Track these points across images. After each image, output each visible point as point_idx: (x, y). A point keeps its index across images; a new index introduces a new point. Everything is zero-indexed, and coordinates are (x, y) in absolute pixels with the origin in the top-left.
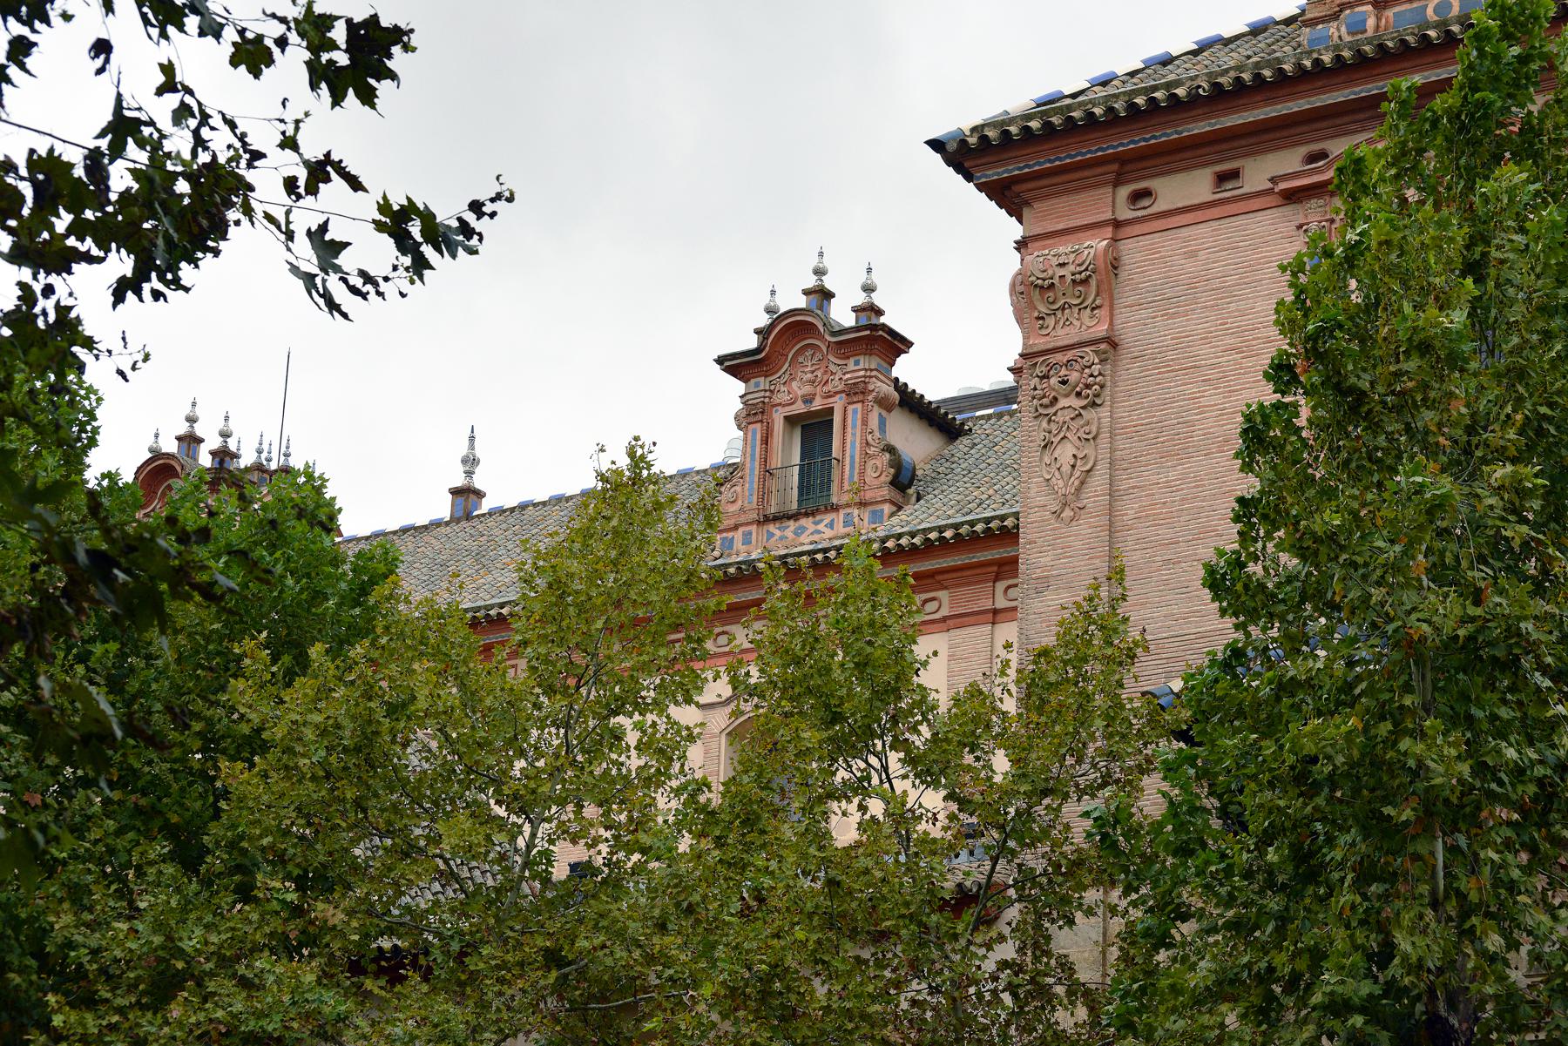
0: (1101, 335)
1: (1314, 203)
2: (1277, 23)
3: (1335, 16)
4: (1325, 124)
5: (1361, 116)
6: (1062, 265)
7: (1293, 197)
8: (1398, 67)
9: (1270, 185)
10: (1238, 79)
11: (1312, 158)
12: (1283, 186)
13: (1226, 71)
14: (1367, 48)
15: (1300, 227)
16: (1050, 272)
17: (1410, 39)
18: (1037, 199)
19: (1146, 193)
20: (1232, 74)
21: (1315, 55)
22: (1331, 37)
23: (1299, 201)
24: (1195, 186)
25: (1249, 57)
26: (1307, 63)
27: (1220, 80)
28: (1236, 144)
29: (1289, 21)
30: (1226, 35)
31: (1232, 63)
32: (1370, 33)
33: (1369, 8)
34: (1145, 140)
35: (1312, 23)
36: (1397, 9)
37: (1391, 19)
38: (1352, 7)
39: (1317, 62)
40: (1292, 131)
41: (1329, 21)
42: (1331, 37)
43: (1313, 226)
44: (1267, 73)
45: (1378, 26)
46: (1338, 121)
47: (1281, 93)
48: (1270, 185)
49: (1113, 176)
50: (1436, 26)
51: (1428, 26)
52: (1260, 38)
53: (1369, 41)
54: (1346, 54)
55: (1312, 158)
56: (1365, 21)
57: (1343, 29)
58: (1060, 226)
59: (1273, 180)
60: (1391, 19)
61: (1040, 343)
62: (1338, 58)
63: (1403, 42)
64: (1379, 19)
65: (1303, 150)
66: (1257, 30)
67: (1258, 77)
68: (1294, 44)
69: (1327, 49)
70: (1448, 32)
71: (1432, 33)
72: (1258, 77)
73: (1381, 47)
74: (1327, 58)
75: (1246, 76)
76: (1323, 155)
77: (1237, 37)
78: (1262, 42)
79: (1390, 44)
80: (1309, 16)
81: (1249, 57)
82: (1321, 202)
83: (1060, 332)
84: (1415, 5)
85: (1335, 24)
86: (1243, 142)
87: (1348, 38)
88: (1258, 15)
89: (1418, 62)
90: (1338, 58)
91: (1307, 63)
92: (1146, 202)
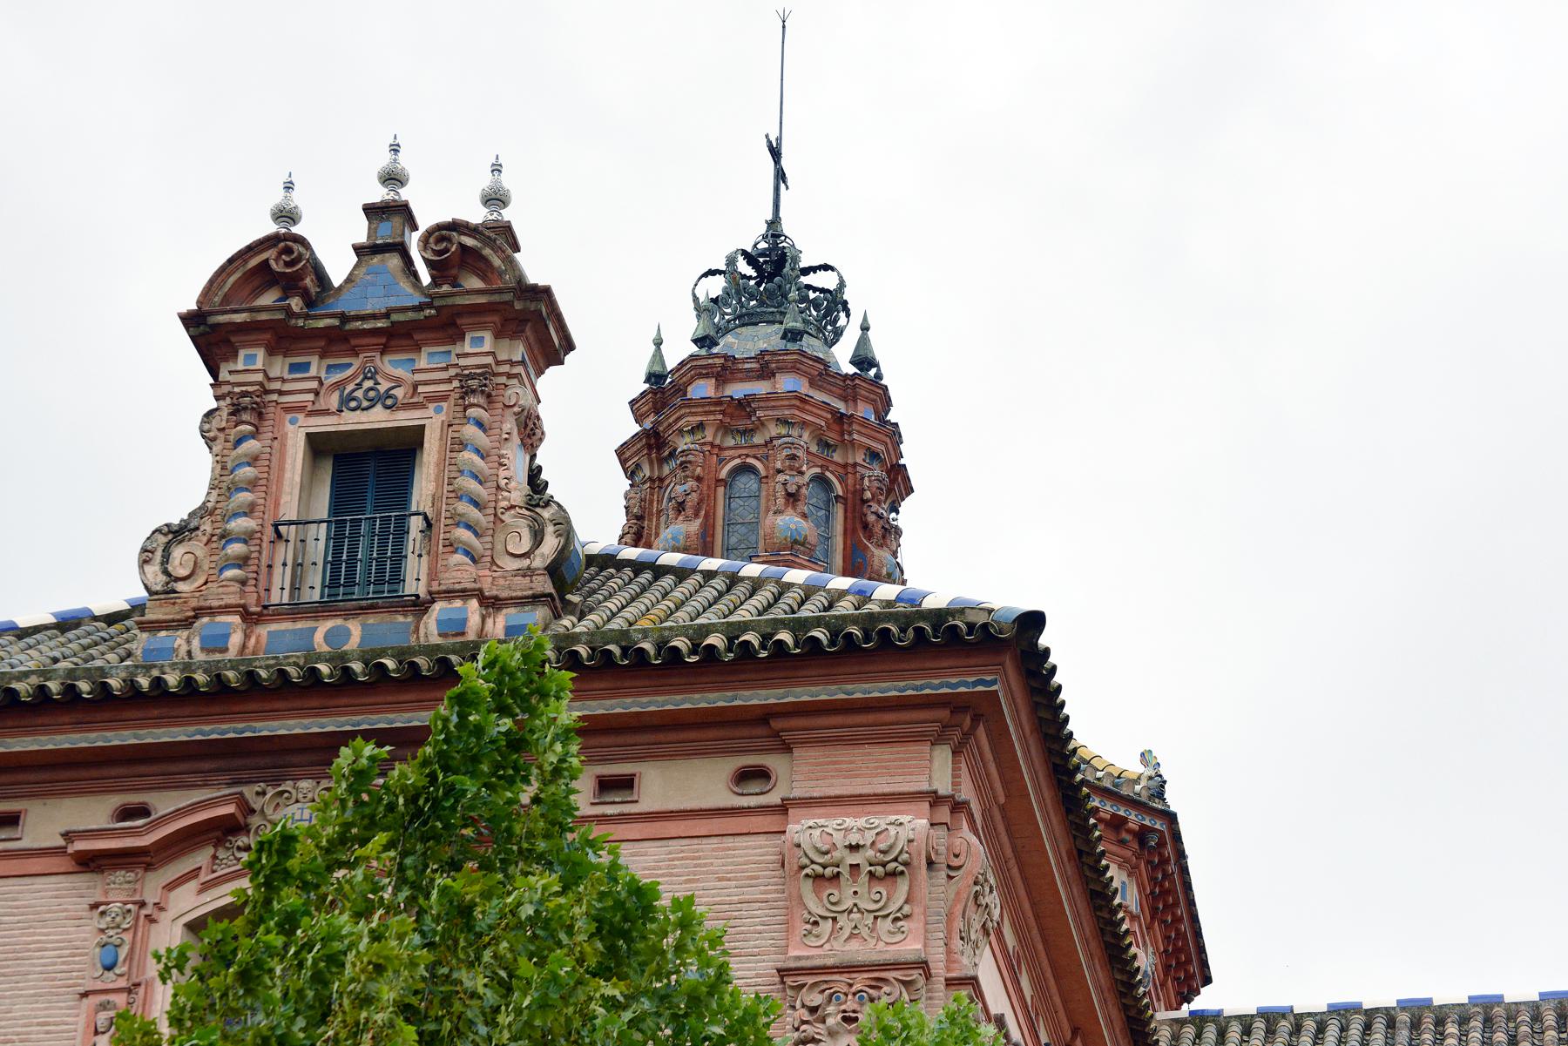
0: (911, 957)
1: (120, 876)
2: (96, 618)
3: (187, 623)
4: (155, 768)
5: (207, 765)
6: (854, 848)
7: (90, 863)
8: (268, 706)
9: (62, 842)
10: (42, 689)
11: (126, 813)
12: (81, 845)
13: (26, 674)
14: (231, 674)
15: (95, 906)
16: (837, 855)
17: (292, 671)
18: (805, 743)
19: (762, 774)
20: (34, 680)
21: (155, 673)
22: (175, 650)
23: (99, 870)
24: (703, 782)
25: (55, 660)
26: (144, 682)
27: (15, 685)
28: (21, 777)
29: (112, 619)
30: (23, 622)
31: (32, 665)
32: (232, 654)
33: (236, 619)
34: (949, 685)
35: (152, 627)
36: (274, 627)
37: (264, 640)
38: (212, 614)
39: (158, 682)
40: (105, 772)
41: (176, 628)
42: (175, 650)
43: (115, 908)
44: (84, 686)
45: (244, 646)
46: (173, 768)
47: (98, 717)
48: (62, 842)
49: (936, 727)
50: (329, 659)
51: (320, 658)
52: (71, 635)
53: (234, 665)
54: (200, 677)
55: (126, 813)
56: (227, 636)
57: (196, 643)
58: (887, 789)
59: (68, 836)
60: (264, 640)
61: (802, 952)
62: (188, 682)
63: (282, 673)
64: (247, 636)
65: (116, 800)
66: (66, 624)
67: (70, 690)
68: (121, 651)
69: (173, 666)
70: (347, 670)
71: (324, 668)
72: (70, 690)
73: (251, 676)
74: (172, 679)
75: (54, 686)
76: (142, 811)
77: (37, 629)
78: (74, 641)
79: (263, 674)
80: (149, 616)
81: (55, 660)
82: (131, 876)
83: (837, 945)
84: (300, 625)
85: (185, 633)
86: (32, 777)
87: (200, 656)
88: (70, 603)
89: (298, 704)
90: (188, 682)
91: (144, 682)
92: (754, 787)
